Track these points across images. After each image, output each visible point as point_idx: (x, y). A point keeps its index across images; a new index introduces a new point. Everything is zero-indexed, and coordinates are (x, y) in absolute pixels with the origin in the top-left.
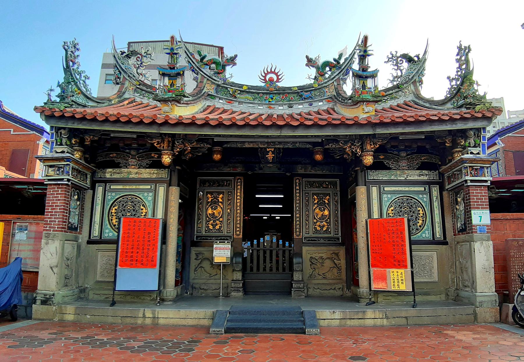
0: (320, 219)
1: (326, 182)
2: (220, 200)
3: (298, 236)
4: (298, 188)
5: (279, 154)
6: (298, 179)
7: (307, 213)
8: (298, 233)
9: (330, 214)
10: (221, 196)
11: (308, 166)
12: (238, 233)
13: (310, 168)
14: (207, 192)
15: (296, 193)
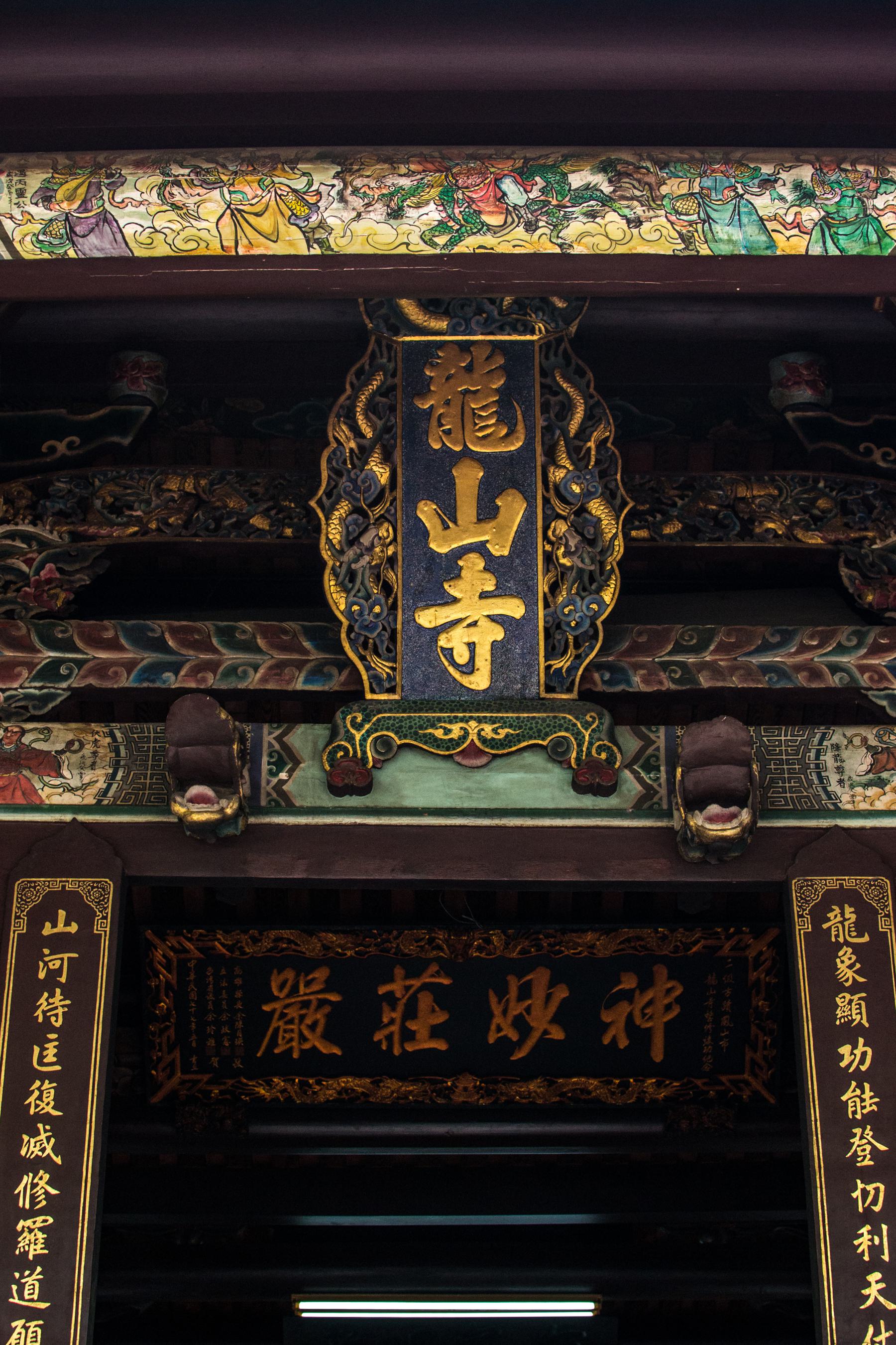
5: (590, 583)
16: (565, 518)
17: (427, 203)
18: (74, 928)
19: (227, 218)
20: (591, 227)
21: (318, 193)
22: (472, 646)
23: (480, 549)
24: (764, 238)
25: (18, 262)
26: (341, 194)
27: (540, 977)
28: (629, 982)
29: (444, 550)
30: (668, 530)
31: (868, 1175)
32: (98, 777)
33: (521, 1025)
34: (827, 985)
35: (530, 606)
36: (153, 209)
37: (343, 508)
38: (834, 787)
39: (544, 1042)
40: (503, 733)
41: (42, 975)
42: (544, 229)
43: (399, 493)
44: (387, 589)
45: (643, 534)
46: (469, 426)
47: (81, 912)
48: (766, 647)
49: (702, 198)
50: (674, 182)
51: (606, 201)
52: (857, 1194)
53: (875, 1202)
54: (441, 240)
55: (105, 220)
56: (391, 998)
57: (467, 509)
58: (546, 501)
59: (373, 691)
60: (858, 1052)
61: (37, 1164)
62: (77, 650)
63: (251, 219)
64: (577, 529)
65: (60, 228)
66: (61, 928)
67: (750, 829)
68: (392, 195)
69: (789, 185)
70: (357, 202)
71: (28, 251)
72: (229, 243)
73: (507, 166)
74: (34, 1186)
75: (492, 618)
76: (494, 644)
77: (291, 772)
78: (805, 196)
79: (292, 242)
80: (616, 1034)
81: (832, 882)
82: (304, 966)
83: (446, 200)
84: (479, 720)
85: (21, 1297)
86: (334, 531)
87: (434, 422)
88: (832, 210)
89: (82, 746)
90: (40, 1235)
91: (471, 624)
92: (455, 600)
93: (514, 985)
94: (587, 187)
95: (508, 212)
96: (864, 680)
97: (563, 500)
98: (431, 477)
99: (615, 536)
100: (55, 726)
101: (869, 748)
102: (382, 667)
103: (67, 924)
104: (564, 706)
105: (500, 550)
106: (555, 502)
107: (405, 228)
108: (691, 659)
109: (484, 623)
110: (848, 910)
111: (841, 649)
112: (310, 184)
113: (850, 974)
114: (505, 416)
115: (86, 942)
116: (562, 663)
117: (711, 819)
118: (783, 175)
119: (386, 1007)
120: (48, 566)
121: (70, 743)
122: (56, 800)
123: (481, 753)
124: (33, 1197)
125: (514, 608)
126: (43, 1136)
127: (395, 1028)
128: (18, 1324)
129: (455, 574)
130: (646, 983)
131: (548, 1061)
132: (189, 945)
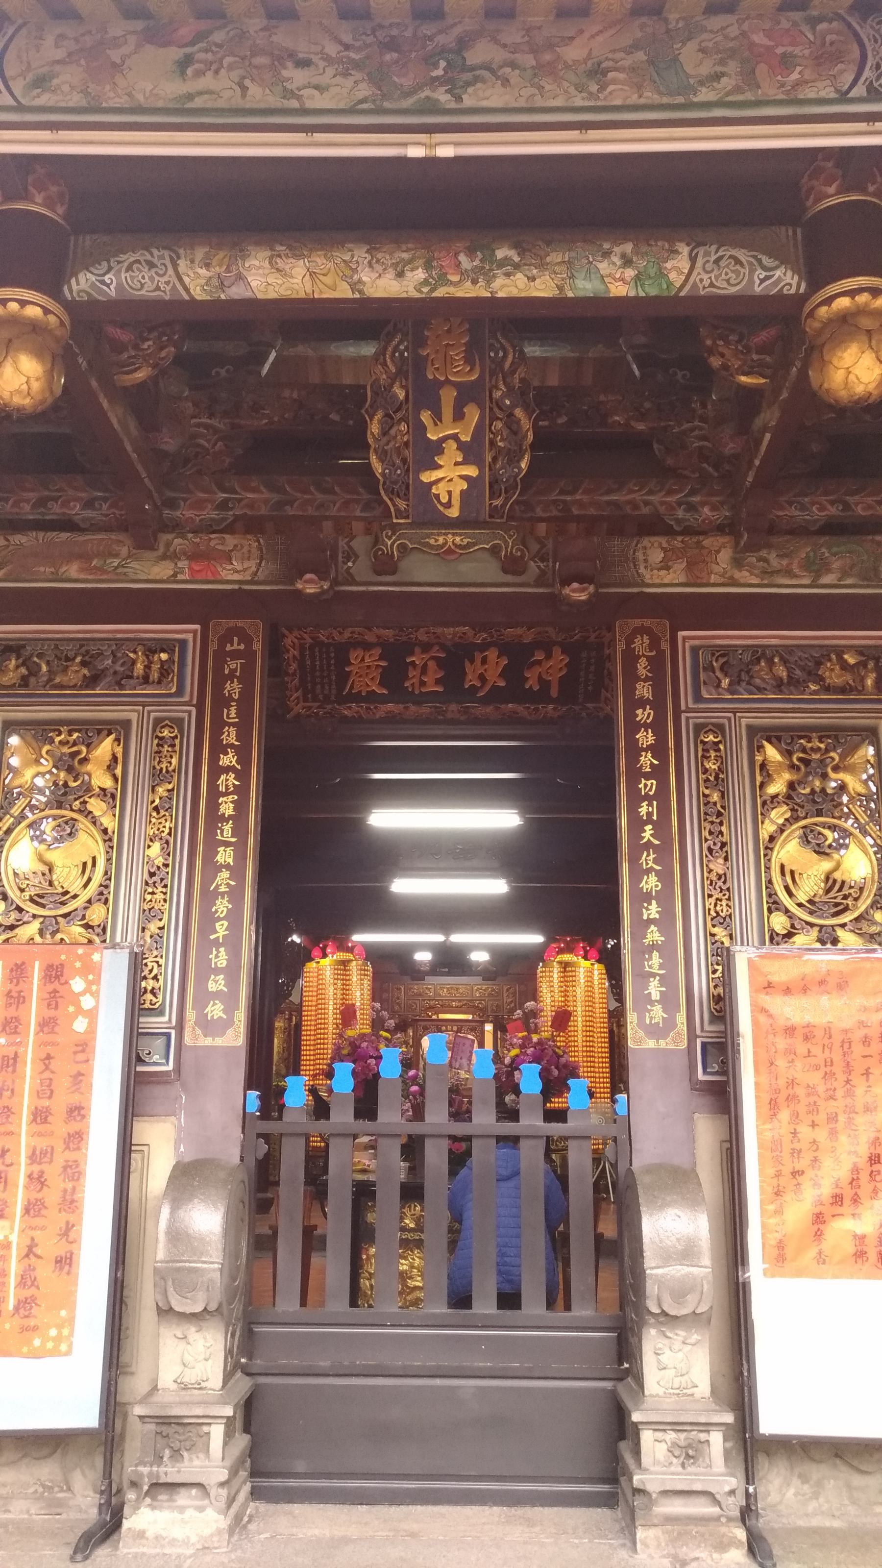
1: (840, 651)
3: (655, 1031)
4: (644, 690)
5: (514, 457)
7: (718, 866)
8: (657, 1013)
10: (106, 747)
12: (216, 1010)
13: (725, 556)
14: (752, 730)
15: (633, 727)
16: (501, 420)
17: (417, 268)
18: (242, 647)
19: (307, 277)
20: (507, 281)
21: (357, 262)
22: (450, 493)
23: (455, 437)
24: (603, 287)
25: (193, 301)
26: (370, 263)
27: (492, 654)
28: (539, 656)
29: (434, 438)
30: (560, 421)
31: (647, 776)
32: (252, 564)
33: (482, 678)
34: (632, 678)
35: (481, 469)
36: (266, 271)
37: (379, 415)
38: (642, 570)
39: (494, 687)
40: (466, 541)
41: (227, 672)
42: (481, 283)
43: (410, 405)
44: (404, 461)
45: (546, 423)
46: (449, 366)
47: (246, 639)
48: (609, 492)
49: (569, 264)
50: (554, 255)
51: (517, 267)
52: (641, 786)
53: (650, 790)
54: (425, 290)
55: (240, 278)
56: (413, 663)
57: (447, 412)
58: (491, 409)
59: (397, 518)
60: (646, 713)
61: (228, 769)
62: (236, 493)
63: (321, 277)
64: (508, 426)
65: (215, 282)
66: (235, 647)
67: (596, 594)
68: (397, 264)
69: (619, 255)
70: (379, 268)
71: (199, 294)
72: (309, 291)
73: (460, 245)
74: (227, 780)
75: (461, 477)
76: (462, 492)
77: (354, 563)
78: (627, 262)
79: (344, 291)
80: (532, 683)
81: (637, 622)
82: (367, 646)
83: (428, 266)
84: (453, 534)
85: (222, 836)
86: (375, 428)
87: (429, 363)
88: (642, 270)
89: (242, 547)
90: (231, 805)
91: (449, 479)
92: (441, 467)
93: (478, 656)
94: (506, 258)
95: (462, 274)
96: (662, 509)
97: (500, 409)
98: (427, 396)
99: (528, 430)
100: (227, 536)
101: (662, 548)
102: (402, 504)
103: (239, 644)
104: (499, 526)
105: (466, 438)
106: (496, 410)
107: (405, 283)
108: (569, 498)
109: (456, 479)
110: (645, 637)
111: (651, 492)
112: (353, 256)
113: (644, 672)
114: (469, 360)
115: (248, 655)
116: (497, 502)
117: (574, 591)
118: (616, 249)
119: (410, 668)
120: (220, 443)
121: (236, 546)
122: (230, 578)
123: (454, 552)
124: (227, 786)
125: (472, 471)
126: (231, 755)
127: (414, 680)
128: (221, 849)
129: (440, 451)
130: (549, 656)
131: (496, 696)
132: (305, 636)
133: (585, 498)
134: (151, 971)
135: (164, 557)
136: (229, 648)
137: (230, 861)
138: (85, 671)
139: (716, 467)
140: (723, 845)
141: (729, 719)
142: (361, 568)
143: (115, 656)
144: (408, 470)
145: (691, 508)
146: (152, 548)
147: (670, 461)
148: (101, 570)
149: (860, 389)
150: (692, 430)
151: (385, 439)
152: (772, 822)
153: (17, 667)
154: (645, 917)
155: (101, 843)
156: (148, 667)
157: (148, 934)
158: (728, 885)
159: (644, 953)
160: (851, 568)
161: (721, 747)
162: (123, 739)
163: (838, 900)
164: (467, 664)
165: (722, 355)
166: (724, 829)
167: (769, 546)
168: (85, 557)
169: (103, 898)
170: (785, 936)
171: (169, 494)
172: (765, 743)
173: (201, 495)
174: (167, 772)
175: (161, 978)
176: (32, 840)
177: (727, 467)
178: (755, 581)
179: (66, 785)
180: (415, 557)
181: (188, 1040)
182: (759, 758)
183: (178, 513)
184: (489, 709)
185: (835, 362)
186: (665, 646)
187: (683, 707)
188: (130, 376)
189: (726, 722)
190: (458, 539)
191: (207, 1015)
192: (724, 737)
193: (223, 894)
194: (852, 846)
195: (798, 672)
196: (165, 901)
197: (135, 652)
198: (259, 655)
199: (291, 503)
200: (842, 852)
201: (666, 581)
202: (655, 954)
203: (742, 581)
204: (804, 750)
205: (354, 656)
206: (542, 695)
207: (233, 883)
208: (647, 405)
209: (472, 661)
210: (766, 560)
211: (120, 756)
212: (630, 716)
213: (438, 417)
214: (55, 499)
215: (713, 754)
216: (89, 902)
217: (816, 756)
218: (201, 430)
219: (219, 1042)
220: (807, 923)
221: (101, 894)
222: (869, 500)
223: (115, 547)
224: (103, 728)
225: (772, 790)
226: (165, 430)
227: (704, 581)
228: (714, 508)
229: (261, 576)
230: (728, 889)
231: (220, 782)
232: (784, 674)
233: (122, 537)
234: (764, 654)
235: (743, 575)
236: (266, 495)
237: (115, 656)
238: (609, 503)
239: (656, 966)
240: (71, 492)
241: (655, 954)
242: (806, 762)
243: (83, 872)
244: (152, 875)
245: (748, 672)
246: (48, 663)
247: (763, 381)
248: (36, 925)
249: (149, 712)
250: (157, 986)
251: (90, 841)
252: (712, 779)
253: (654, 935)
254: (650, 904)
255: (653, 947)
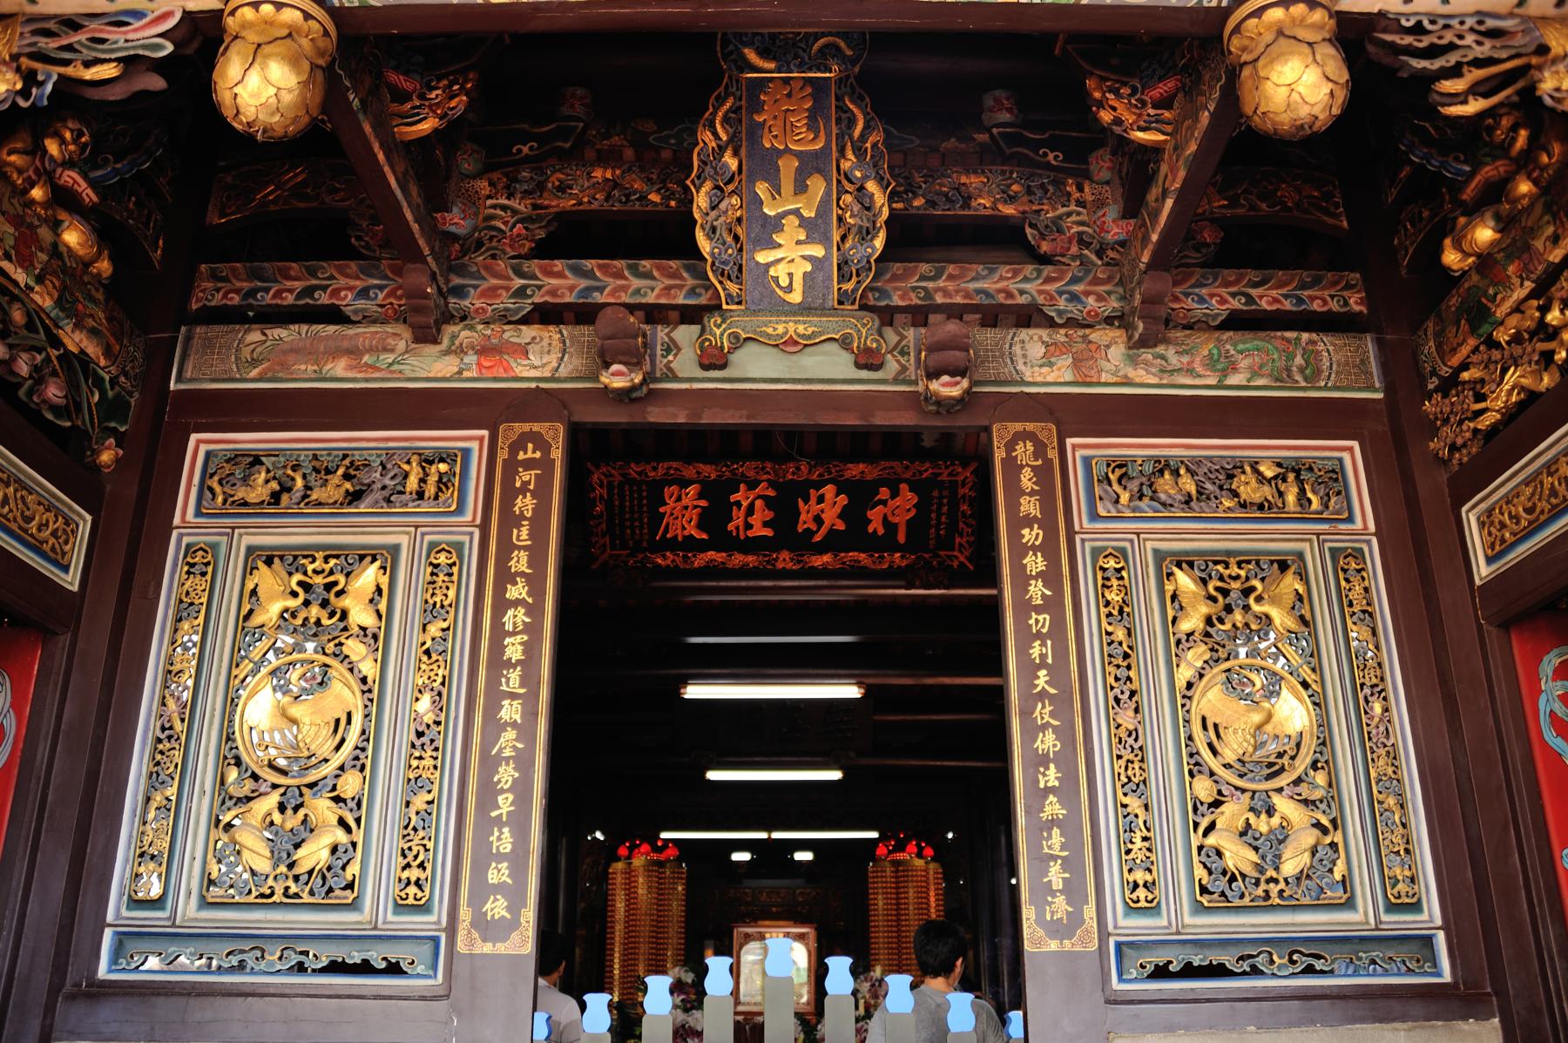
0: (1242, 767)
2: (360, 616)
3: (1059, 930)
4: (1030, 506)
5: (866, 234)
6: (1031, 436)
7: (1127, 719)
8: (1060, 906)
9: (1324, 724)
10: (369, 576)
11: (1099, 336)
12: (497, 908)
14: (1160, 556)
15: (1020, 550)
18: (538, 455)
22: (790, 275)
23: (796, 212)
27: (829, 490)
28: (884, 493)
32: (553, 359)
34: (1015, 491)
35: (828, 249)
37: (708, 186)
38: (1021, 367)
40: (810, 330)
41: (518, 484)
43: (744, 176)
44: (736, 238)
52: (1032, 622)
57: (787, 185)
58: (839, 182)
61: (516, 603)
62: (537, 278)
66: (530, 455)
67: (968, 392)
80: (876, 526)
86: (701, 200)
91: (790, 260)
96: (1040, 300)
102: (733, 288)
105: (808, 213)
106: (845, 182)
108: (930, 285)
111: (1026, 279)
113: (1030, 484)
114: (812, 126)
115: (546, 464)
117: (944, 385)
121: (534, 338)
122: (526, 374)
123: (796, 343)
125: (818, 251)
128: (506, 703)
129: (779, 228)
131: (834, 542)
133: (951, 286)
134: (416, 857)
135: (447, 352)
136: (521, 456)
137: (518, 718)
138: (348, 485)
139: (1100, 253)
140: (1133, 693)
141: (1131, 541)
142: (685, 363)
143: (384, 468)
144: (741, 250)
145: (1074, 298)
146: (435, 342)
147: (1045, 247)
148: (374, 368)
149: (1304, 112)
150: (1069, 214)
151: (713, 214)
152: (1190, 664)
153: (267, 481)
154: (1042, 785)
155: (358, 694)
156: (423, 481)
157: (413, 809)
158: (1140, 742)
159: (1041, 830)
160: (1261, 367)
161: (1124, 574)
162: (390, 568)
163: (1272, 759)
164: (801, 503)
165: (1114, 109)
166: (1132, 674)
167: (1166, 341)
168: (354, 352)
169: (359, 764)
170: (1210, 805)
171: (457, 281)
172: (1176, 570)
173: (495, 282)
174: (442, 607)
175: (429, 866)
176: (274, 690)
177: (1111, 254)
178: (1154, 380)
179: (318, 623)
180: (751, 348)
181: (461, 947)
182: (1169, 588)
183: (467, 303)
184: (827, 558)
185: (1274, 77)
186: (1053, 454)
187: (1077, 528)
188: (414, 128)
189: (1127, 545)
190: (801, 329)
191: (485, 914)
192: (1126, 561)
193: (507, 759)
194: (1284, 692)
195: (1208, 486)
196: (435, 767)
197: (408, 462)
198: (558, 464)
199: (601, 289)
200: (1273, 700)
201: (1050, 379)
202: (1056, 832)
203: (1138, 380)
204: (1221, 578)
205: (670, 491)
206: (887, 542)
207: (520, 746)
208: (1015, 187)
209: (806, 501)
210: (1163, 357)
211: (385, 588)
212: (1015, 536)
213: (776, 189)
214: (324, 288)
215: (1115, 582)
216: (342, 768)
217: (1236, 585)
218: (499, 212)
219: (502, 948)
220: (1237, 788)
221: (357, 758)
222: (1274, 293)
223: (391, 341)
224: (367, 555)
225: (1185, 626)
226: (455, 210)
227: (1094, 380)
228: (1100, 298)
229: (563, 372)
230: (1141, 748)
231: (506, 619)
232: (1193, 489)
233: (400, 328)
234: (1167, 465)
235: (1139, 374)
236: (572, 280)
237: (384, 468)
238: (978, 292)
239: (1057, 846)
240: (343, 281)
241: (1056, 832)
242: (1225, 593)
243: (336, 731)
244: (420, 734)
245: (1150, 486)
246: (304, 477)
247: (1162, 137)
248: (274, 798)
249: (423, 534)
250: (423, 876)
251: (346, 692)
252: (1115, 612)
253: (1053, 807)
254: (1047, 768)
255: (1054, 822)
